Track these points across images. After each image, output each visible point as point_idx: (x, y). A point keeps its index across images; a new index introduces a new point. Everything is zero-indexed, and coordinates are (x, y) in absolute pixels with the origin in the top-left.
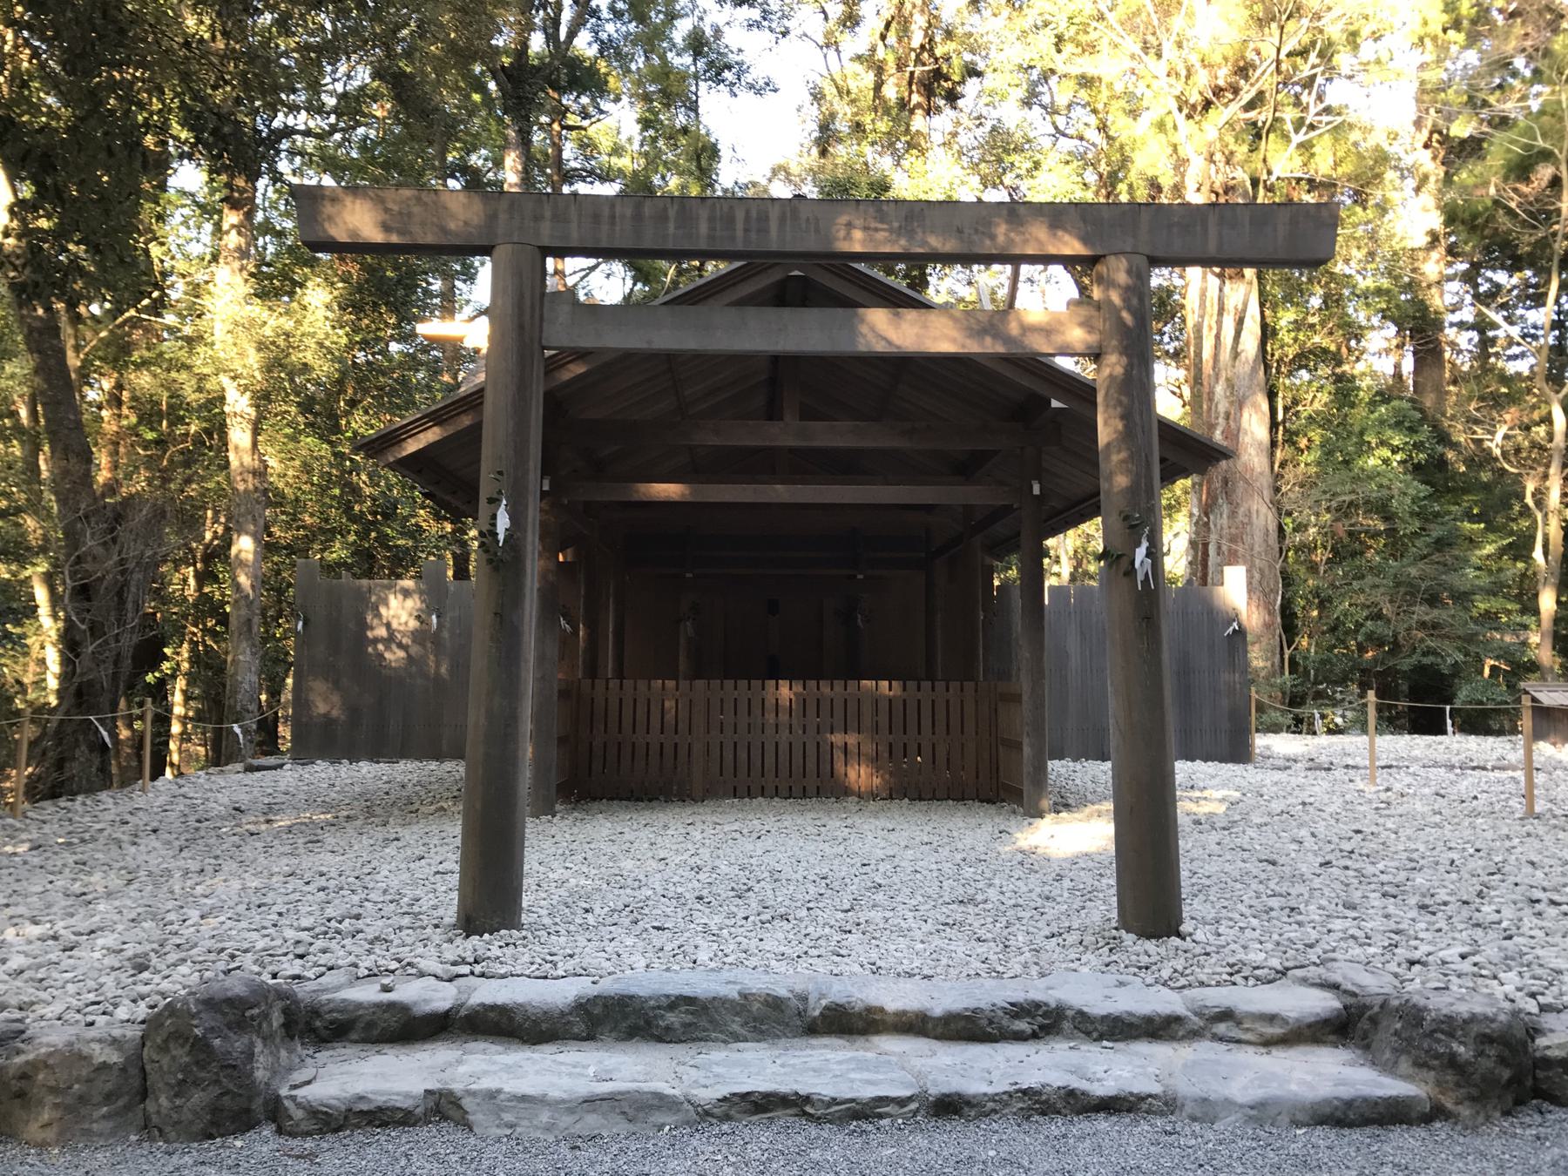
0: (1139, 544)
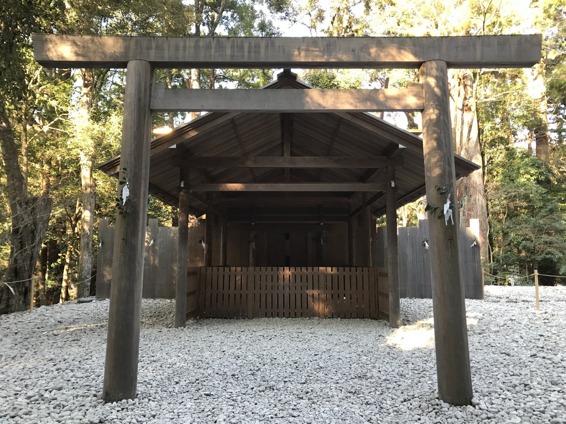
0: (446, 202)
